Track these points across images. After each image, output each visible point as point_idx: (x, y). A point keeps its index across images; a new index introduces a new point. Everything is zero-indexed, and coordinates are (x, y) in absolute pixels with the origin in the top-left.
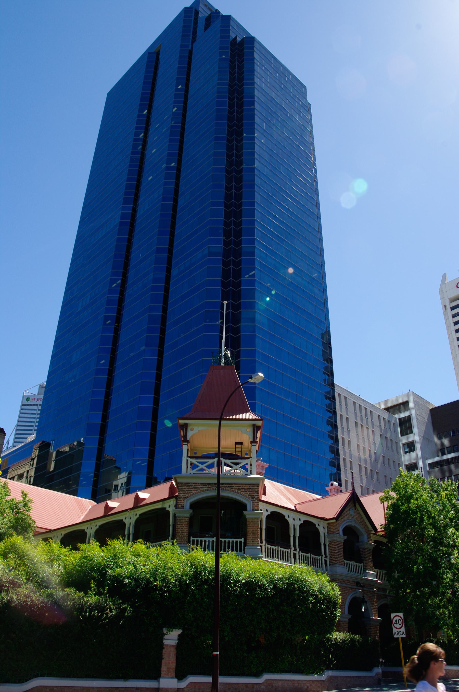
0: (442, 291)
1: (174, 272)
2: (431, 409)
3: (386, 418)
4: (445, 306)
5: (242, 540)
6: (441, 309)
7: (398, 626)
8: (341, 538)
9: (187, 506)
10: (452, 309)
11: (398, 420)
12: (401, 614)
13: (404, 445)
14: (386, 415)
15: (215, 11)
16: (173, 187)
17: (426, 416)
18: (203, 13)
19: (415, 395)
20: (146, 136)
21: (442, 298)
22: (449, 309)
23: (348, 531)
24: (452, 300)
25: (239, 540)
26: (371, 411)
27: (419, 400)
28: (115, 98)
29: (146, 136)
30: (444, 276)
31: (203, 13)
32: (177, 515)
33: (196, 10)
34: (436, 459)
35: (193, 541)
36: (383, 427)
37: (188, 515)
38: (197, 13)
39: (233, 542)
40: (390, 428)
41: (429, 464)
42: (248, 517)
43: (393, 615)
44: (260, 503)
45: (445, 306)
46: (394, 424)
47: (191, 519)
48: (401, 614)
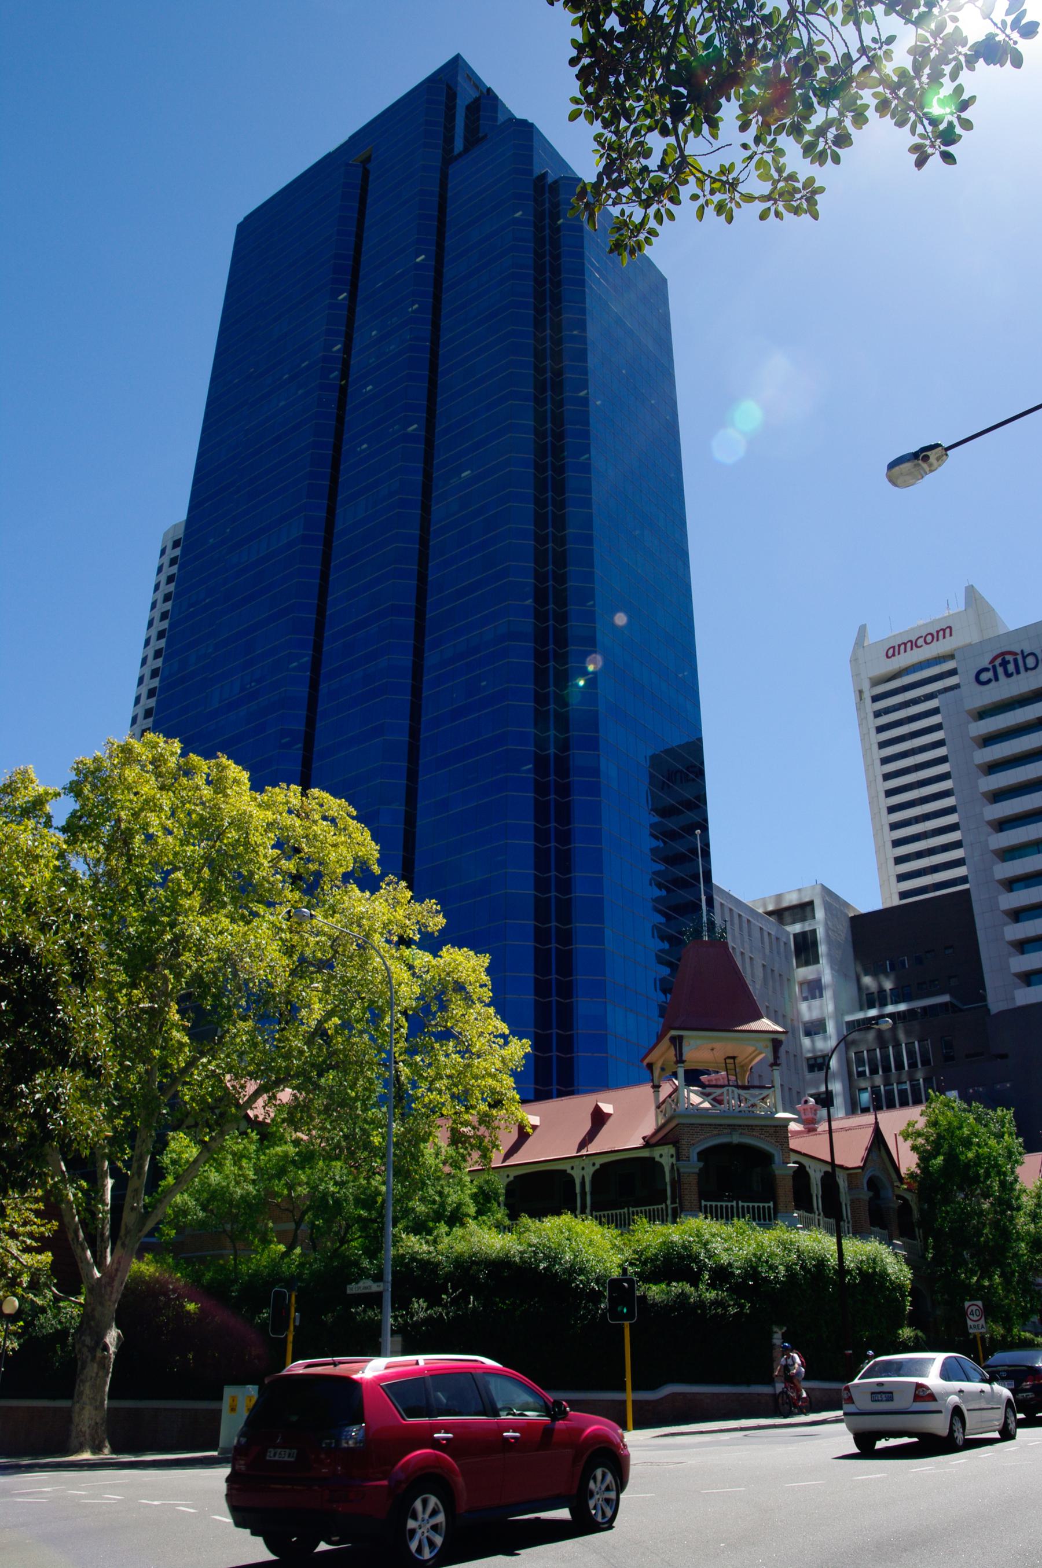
0: (856, 660)
1: (431, 658)
2: (852, 918)
3: (773, 933)
4: (861, 692)
5: (771, 1204)
6: (850, 698)
7: (975, 1318)
8: (865, 1195)
9: (694, 1156)
10: (875, 699)
11: (792, 937)
12: (980, 1303)
13: (801, 984)
14: (771, 926)
15: (485, 91)
16: (419, 478)
17: (844, 931)
18: (465, 96)
19: (826, 891)
20: (347, 348)
21: (856, 675)
22: (868, 700)
23: (873, 1184)
24: (876, 682)
25: (766, 1205)
26: (748, 921)
27: (833, 902)
28: (261, 236)
29: (347, 348)
30: (862, 630)
31: (465, 96)
32: (681, 1170)
33: (449, 87)
34: (860, 1016)
35: (706, 1206)
36: (767, 951)
37: (697, 1170)
38: (452, 96)
39: (759, 1207)
40: (779, 953)
41: (848, 1023)
42: (777, 1172)
43: (967, 1304)
44: (792, 1153)
45: (861, 692)
46: (785, 944)
47: (703, 1174)
48: (980, 1303)
